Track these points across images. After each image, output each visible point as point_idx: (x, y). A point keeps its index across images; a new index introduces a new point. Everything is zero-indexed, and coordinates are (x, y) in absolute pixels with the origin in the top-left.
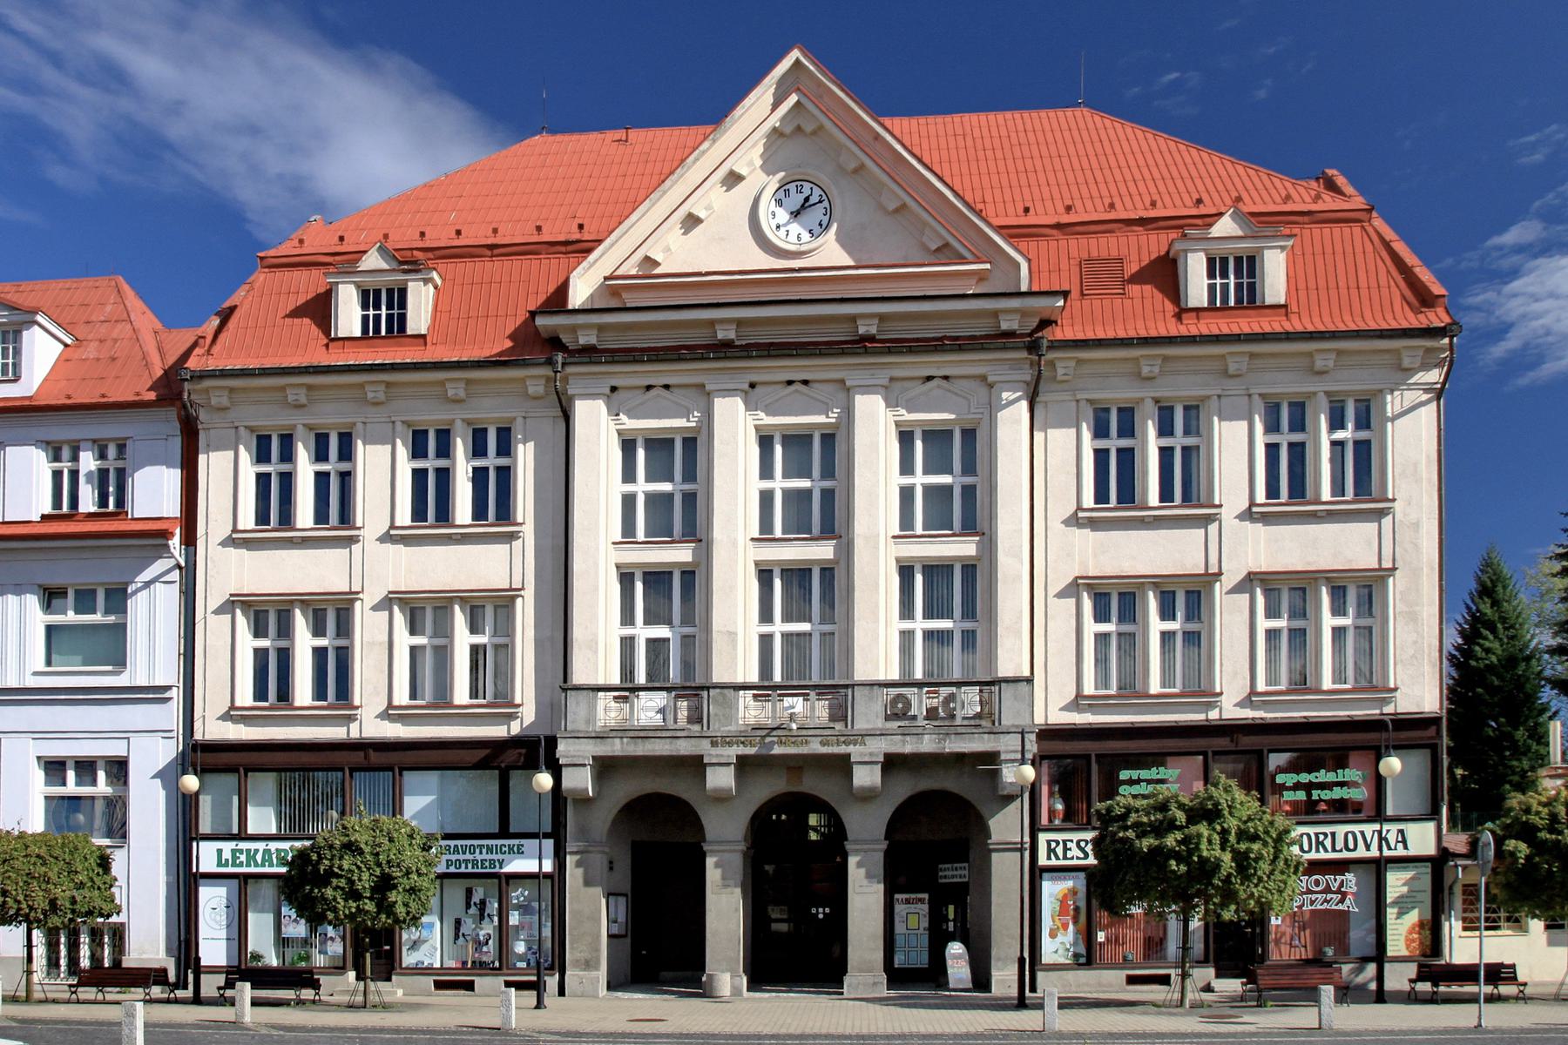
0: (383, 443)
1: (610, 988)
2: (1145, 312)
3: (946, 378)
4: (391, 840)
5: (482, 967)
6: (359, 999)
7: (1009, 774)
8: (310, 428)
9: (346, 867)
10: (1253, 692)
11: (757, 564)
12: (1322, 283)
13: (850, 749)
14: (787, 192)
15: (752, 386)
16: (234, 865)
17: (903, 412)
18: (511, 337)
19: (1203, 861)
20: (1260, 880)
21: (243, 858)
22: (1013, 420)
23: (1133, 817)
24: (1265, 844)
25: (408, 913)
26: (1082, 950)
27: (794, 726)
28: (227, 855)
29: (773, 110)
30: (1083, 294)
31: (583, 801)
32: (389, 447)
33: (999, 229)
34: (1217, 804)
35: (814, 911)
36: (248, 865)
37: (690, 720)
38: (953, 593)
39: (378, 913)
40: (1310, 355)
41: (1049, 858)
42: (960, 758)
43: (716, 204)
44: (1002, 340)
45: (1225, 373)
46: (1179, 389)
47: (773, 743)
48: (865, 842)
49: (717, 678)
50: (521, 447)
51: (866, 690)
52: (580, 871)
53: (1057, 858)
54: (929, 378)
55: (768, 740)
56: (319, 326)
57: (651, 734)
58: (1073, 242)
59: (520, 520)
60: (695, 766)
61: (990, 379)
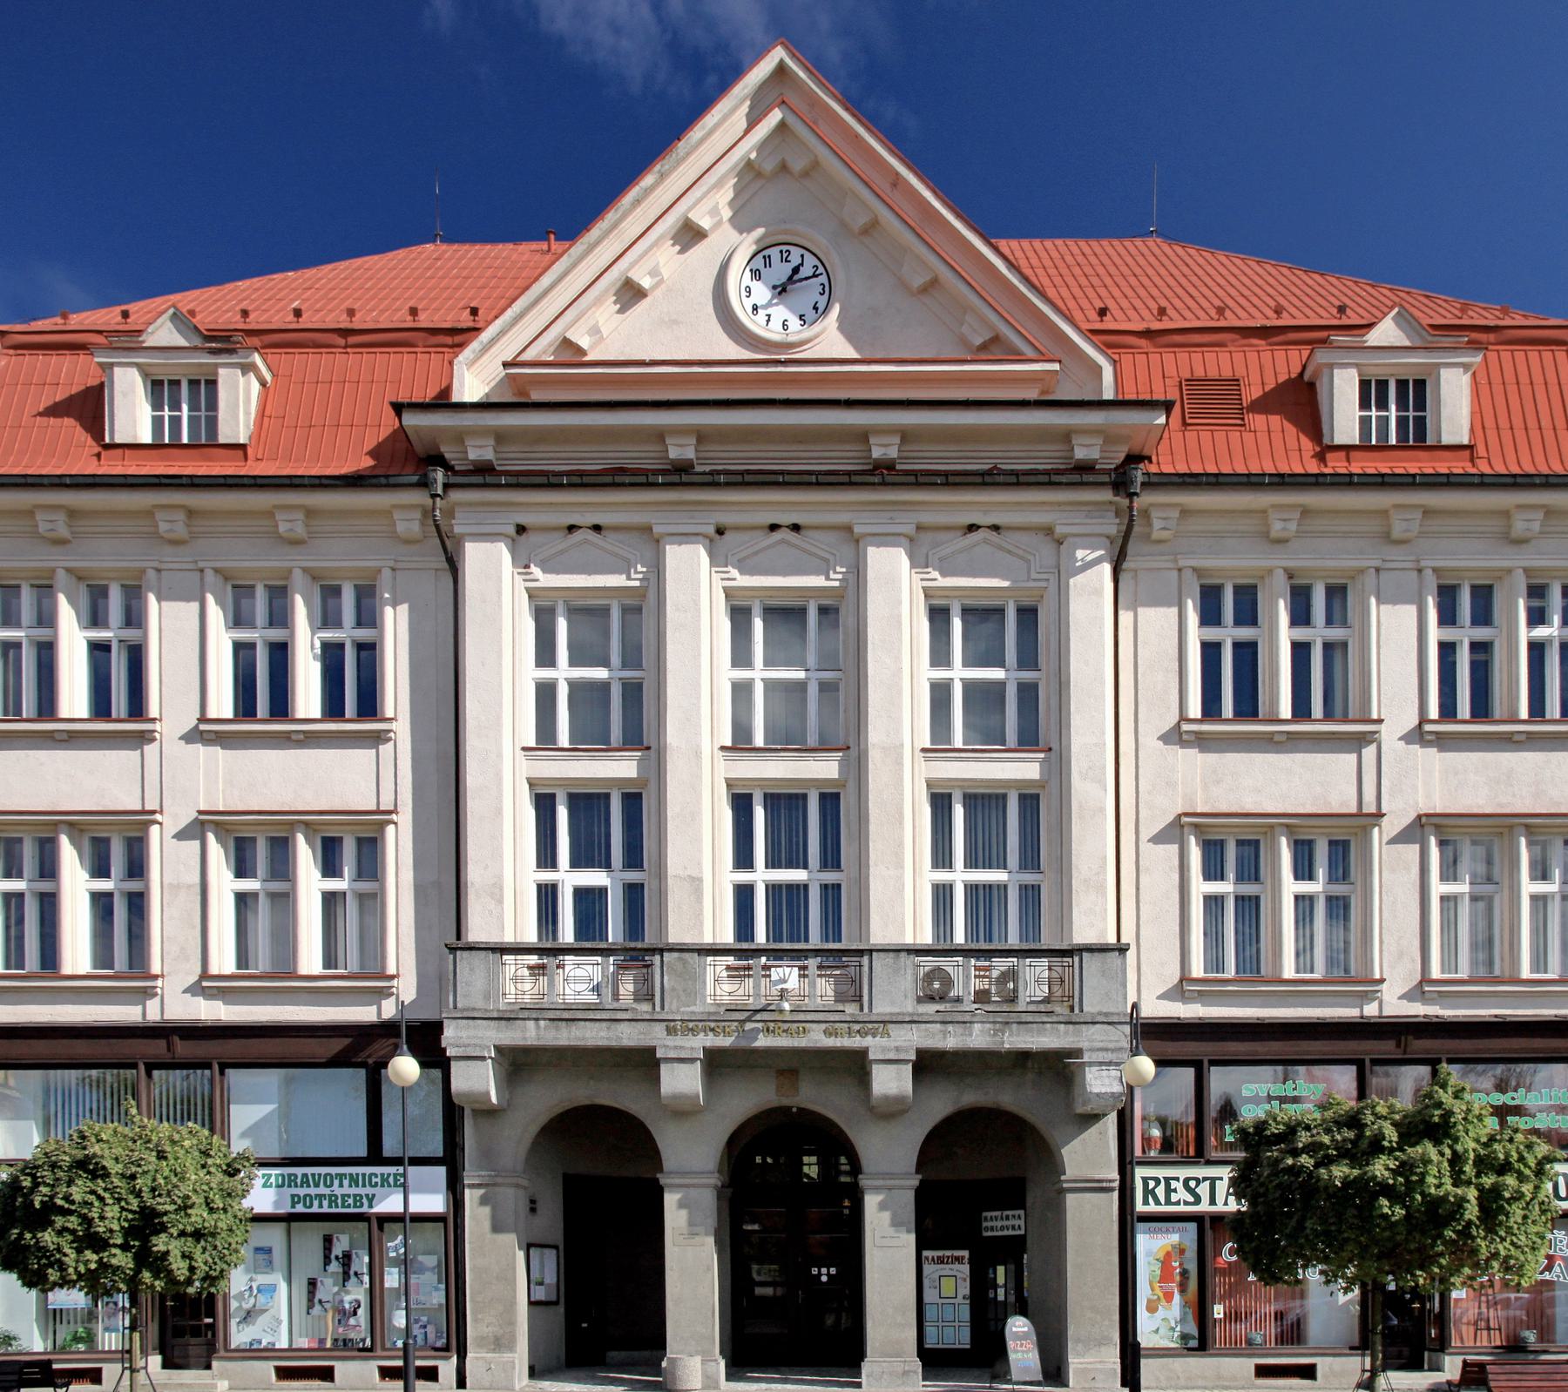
0: (187, 598)
1: (534, 1373)
2: (1274, 444)
3: (996, 528)
4: (161, 1156)
5: (346, 1347)
7: (1100, 1082)
8: (78, 576)
9: (77, 1197)
10: (1425, 979)
11: (730, 783)
12: (1518, 421)
13: (868, 1041)
14: (767, 261)
15: (720, 531)
17: (935, 574)
18: (373, 453)
19: (1434, 1203)
20: (1509, 1230)
22: (1090, 591)
23: (1303, 1138)
24: (1521, 1178)
25: (192, 1269)
26: (1193, 1330)
27: (786, 1006)
29: (747, 132)
30: (1185, 424)
31: (488, 1113)
32: (195, 606)
34: (1448, 1114)
35: (815, 1271)
37: (638, 998)
38: (1009, 828)
39: (137, 1271)
40: (1506, 514)
41: (1146, 1202)
42: (1023, 1059)
43: (660, 264)
44: (1081, 473)
45: (1265, 536)
46: (1322, 559)
47: (757, 1031)
48: (891, 1176)
49: (675, 936)
50: (389, 611)
52: (487, 1210)
53: (1158, 1202)
54: (972, 528)
55: (749, 1026)
56: (87, 429)
57: (579, 1015)
58: (1168, 358)
59: (389, 713)
60: (644, 1063)
61: (1059, 530)
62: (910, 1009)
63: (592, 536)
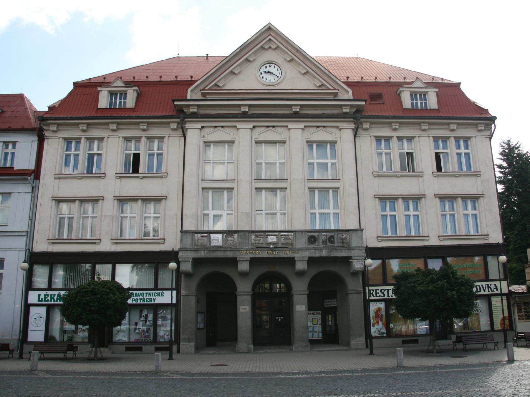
5: (147, 343)
6: (92, 355)
7: (357, 265)
16: (45, 301)
21: (49, 298)
28: (42, 297)
33: (343, 82)
36: (51, 301)
44: (345, 115)
51: (300, 234)
53: (374, 296)
61: (340, 127)
62: (306, 247)
63: (221, 129)
